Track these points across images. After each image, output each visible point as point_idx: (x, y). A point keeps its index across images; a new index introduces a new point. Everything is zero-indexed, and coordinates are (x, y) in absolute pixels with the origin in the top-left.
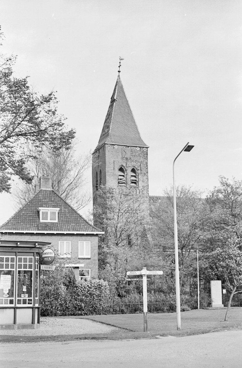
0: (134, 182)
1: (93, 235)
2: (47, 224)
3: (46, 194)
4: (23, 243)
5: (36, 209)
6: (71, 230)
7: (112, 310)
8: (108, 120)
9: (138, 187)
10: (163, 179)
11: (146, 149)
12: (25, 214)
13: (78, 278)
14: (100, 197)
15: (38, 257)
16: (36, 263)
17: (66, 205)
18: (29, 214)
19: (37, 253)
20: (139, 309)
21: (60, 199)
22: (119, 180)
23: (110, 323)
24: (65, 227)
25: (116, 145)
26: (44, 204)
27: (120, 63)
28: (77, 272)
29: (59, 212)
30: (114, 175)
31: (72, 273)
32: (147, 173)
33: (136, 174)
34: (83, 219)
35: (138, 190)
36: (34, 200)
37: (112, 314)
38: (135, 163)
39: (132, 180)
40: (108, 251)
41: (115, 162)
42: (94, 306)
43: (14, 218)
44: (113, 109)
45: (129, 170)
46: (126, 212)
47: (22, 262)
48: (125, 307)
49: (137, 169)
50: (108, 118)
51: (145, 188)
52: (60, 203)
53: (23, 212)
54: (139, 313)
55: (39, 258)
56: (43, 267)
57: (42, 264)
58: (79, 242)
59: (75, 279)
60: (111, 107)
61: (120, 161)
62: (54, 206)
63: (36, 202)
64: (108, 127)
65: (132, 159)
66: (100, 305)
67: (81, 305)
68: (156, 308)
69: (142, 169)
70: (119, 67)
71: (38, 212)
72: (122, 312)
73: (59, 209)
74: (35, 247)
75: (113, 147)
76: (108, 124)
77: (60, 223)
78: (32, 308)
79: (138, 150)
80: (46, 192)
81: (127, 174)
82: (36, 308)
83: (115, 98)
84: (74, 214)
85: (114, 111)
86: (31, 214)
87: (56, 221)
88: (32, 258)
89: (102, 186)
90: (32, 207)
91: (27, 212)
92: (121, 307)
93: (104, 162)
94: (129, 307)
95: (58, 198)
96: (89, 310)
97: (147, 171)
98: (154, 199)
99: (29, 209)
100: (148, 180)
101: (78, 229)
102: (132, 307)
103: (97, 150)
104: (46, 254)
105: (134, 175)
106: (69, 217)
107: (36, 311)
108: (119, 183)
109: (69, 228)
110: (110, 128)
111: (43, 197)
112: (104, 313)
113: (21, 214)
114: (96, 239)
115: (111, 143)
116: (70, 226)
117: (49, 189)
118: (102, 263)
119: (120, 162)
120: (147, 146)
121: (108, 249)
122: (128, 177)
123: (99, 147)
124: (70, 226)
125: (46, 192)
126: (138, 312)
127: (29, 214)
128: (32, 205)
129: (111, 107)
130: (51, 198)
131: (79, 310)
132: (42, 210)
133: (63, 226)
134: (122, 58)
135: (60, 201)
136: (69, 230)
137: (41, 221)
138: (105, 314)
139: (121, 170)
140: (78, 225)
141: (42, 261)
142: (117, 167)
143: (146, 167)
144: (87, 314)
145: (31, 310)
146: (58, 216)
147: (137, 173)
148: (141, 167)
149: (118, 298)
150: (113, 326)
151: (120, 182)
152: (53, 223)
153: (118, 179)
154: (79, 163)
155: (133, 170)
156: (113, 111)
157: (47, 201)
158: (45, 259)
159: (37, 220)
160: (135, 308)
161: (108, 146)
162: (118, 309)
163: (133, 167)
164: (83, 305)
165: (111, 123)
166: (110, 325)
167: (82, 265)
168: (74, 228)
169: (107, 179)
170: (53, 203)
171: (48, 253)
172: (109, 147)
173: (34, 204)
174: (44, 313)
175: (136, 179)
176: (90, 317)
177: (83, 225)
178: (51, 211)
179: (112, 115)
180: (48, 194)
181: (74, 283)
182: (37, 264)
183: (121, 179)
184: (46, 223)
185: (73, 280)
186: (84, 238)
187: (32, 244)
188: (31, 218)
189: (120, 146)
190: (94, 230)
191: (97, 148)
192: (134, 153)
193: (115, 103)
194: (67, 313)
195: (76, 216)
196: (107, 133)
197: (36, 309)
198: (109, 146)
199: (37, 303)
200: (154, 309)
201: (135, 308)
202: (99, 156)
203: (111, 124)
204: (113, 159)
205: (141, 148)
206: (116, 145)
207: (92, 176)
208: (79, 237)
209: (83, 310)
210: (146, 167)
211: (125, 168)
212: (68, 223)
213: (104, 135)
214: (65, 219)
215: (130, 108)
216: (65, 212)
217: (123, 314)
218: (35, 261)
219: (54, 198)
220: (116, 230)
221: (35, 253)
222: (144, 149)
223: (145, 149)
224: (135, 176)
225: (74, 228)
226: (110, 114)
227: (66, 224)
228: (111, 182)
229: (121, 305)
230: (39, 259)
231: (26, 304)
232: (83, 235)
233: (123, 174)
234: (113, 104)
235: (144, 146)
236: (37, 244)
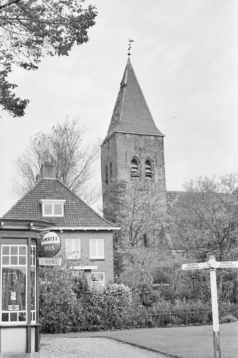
0: (149, 175)
1: (106, 231)
2: (51, 219)
3: (50, 184)
4: (11, 223)
5: (38, 202)
6: (80, 226)
7: (135, 323)
8: (118, 107)
9: (153, 181)
10: (178, 175)
11: (162, 138)
12: (24, 208)
13: (91, 284)
14: (111, 191)
15: (35, 246)
16: (31, 256)
17: (73, 196)
18: (29, 208)
19: (32, 239)
20: (171, 320)
21: (66, 190)
22: (132, 174)
23: (145, 346)
24: (73, 223)
25: (128, 133)
26: (47, 196)
27: (130, 45)
28: (88, 276)
29: (65, 205)
30: (126, 167)
31: (84, 277)
32: (164, 164)
33: (151, 166)
34: (94, 212)
35: (154, 183)
36: (35, 191)
37: (136, 328)
38: (150, 153)
39: (147, 173)
40: (122, 253)
41: (127, 153)
42: (113, 318)
43: (11, 212)
44: (124, 95)
45: (143, 161)
46: (142, 208)
47: (9, 254)
48: (152, 318)
49: (152, 160)
50: (118, 105)
51: (162, 182)
52: (66, 194)
53: (22, 206)
54: (171, 326)
55: (37, 247)
56: (42, 261)
57: (41, 256)
58: (90, 240)
59: (87, 284)
60: (121, 93)
61: (133, 152)
62: (59, 198)
63: (38, 194)
64: (118, 115)
65: (146, 149)
66: (121, 316)
67: (96, 317)
68: (192, 319)
69: (157, 161)
70: (129, 49)
71: (41, 205)
72: (149, 325)
73: (65, 201)
74: (29, 230)
75: (124, 136)
76: (118, 112)
77: (67, 217)
78: (26, 327)
79: (152, 139)
80: (49, 182)
81: (141, 166)
82: (32, 327)
83: (125, 83)
84: (83, 206)
85: (124, 97)
86: (32, 208)
87: (62, 215)
88: (24, 248)
89: (113, 179)
90: (33, 200)
91: (27, 206)
92: (148, 319)
93: (116, 153)
94: (158, 318)
95: (63, 188)
96: (107, 323)
97: (164, 162)
98: (171, 195)
99: (29, 202)
100: (165, 173)
101: (89, 225)
102: (161, 318)
103: (107, 141)
104: (48, 240)
105: (149, 167)
106: (77, 211)
107: (33, 331)
108: (132, 176)
109: (77, 223)
110: (121, 116)
111: (46, 188)
112: (126, 327)
113: (20, 208)
114: (110, 236)
115: (122, 132)
116: (79, 221)
117: (53, 179)
118: (118, 267)
119: (133, 153)
120: (162, 135)
121: (122, 250)
122: (142, 170)
123: (108, 137)
124: (79, 221)
125: (49, 182)
126: (170, 325)
127: (29, 208)
128: (33, 197)
129: (121, 93)
130: (56, 189)
131: (94, 323)
132: (45, 202)
133: (70, 221)
134: (132, 39)
135: (66, 192)
136: (78, 226)
137: (44, 215)
138: (127, 328)
139: (134, 161)
140: (88, 219)
141: (41, 252)
142: (130, 159)
143: (162, 158)
144: (103, 329)
145: (24, 330)
146: (64, 210)
147: (152, 165)
148: (156, 158)
149: (143, 306)
150: (151, 350)
151: (133, 175)
152: (58, 218)
153: (131, 172)
154: (87, 153)
155: (148, 162)
156: (123, 96)
157: (51, 192)
158: (45, 249)
159: (39, 215)
160: (165, 319)
161: (119, 135)
162: (144, 322)
163: (147, 159)
164: (98, 317)
165: (122, 110)
166: (145, 348)
167: (95, 267)
168: (84, 223)
169: (118, 172)
170: (57, 194)
171: (50, 239)
172: (120, 136)
173: (36, 195)
174: (48, 329)
175: (151, 172)
176: (108, 333)
177: (94, 219)
178: (56, 203)
179: (122, 101)
180: (52, 184)
181: (86, 290)
182: (32, 256)
183: (134, 172)
184: (50, 217)
185: (85, 286)
186: (95, 235)
187: (24, 225)
188: (32, 213)
189: (133, 135)
190: (107, 225)
191: (106, 139)
192: (148, 142)
193: (125, 89)
194: (79, 328)
195: (86, 209)
196: (117, 121)
197: (32, 329)
198: (120, 135)
199: (34, 320)
200: (189, 320)
201: (165, 319)
202: (108, 147)
203: (122, 111)
204: (125, 150)
205: (156, 137)
206: (128, 133)
207: (102, 171)
208: (90, 234)
209: (99, 324)
210: (162, 158)
211: (138, 159)
212: (76, 217)
213: (113, 124)
214: (73, 213)
215: (142, 93)
216: (72, 204)
217: (150, 327)
218: (30, 252)
219: (59, 188)
220: (131, 228)
221: (30, 240)
222: (159, 138)
223: (160, 138)
224: (149, 169)
225: (84, 223)
226: (120, 101)
227: (74, 219)
228: (123, 175)
229: (147, 316)
230: (36, 249)
231: (16, 321)
232: (94, 231)
233: (136, 166)
234: (123, 90)
235: (159, 135)
236: (32, 224)
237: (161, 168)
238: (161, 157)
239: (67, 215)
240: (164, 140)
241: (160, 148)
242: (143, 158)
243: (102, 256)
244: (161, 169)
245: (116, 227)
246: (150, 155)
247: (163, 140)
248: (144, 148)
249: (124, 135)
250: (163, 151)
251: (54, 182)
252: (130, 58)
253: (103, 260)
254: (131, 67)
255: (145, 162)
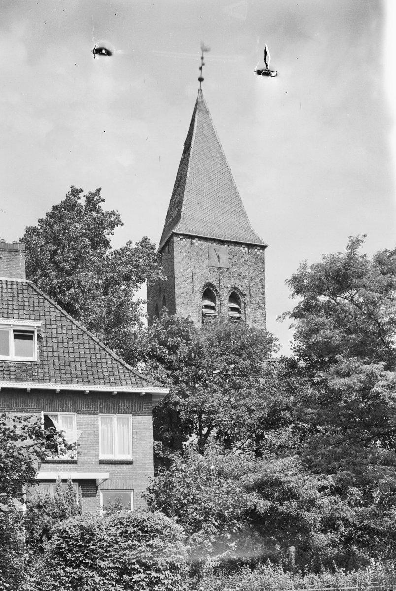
32: (264, 302)
33: (240, 305)
38: (239, 279)
41: (194, 277)
45: (225, 295)
50: (179, 186)
65: (232, 270)
81: (221, 304)
97: (264, 298)
100: (265, 319)
117: (20, 280)
142: (199, 288)
148: (250, 290)
172: (181, 242)
210: (261, 290)
211: (216, 290)
237: (259, 310)
238: (260, 287)
239: (45, 349)
240: (265, 255)
241: (259, 271)
242: (225, 288)
243: (128, 454)
244: (260, 312)
245: (160, 387)
246: (238, 282)
247: (264, 254)
248: (228, 269)
249: (188, 241)
250: (264, 276)
251: (20, 287)
252: (202, 88)
253: (130, 463)
254: (205, 108)
255: (229, 295)
